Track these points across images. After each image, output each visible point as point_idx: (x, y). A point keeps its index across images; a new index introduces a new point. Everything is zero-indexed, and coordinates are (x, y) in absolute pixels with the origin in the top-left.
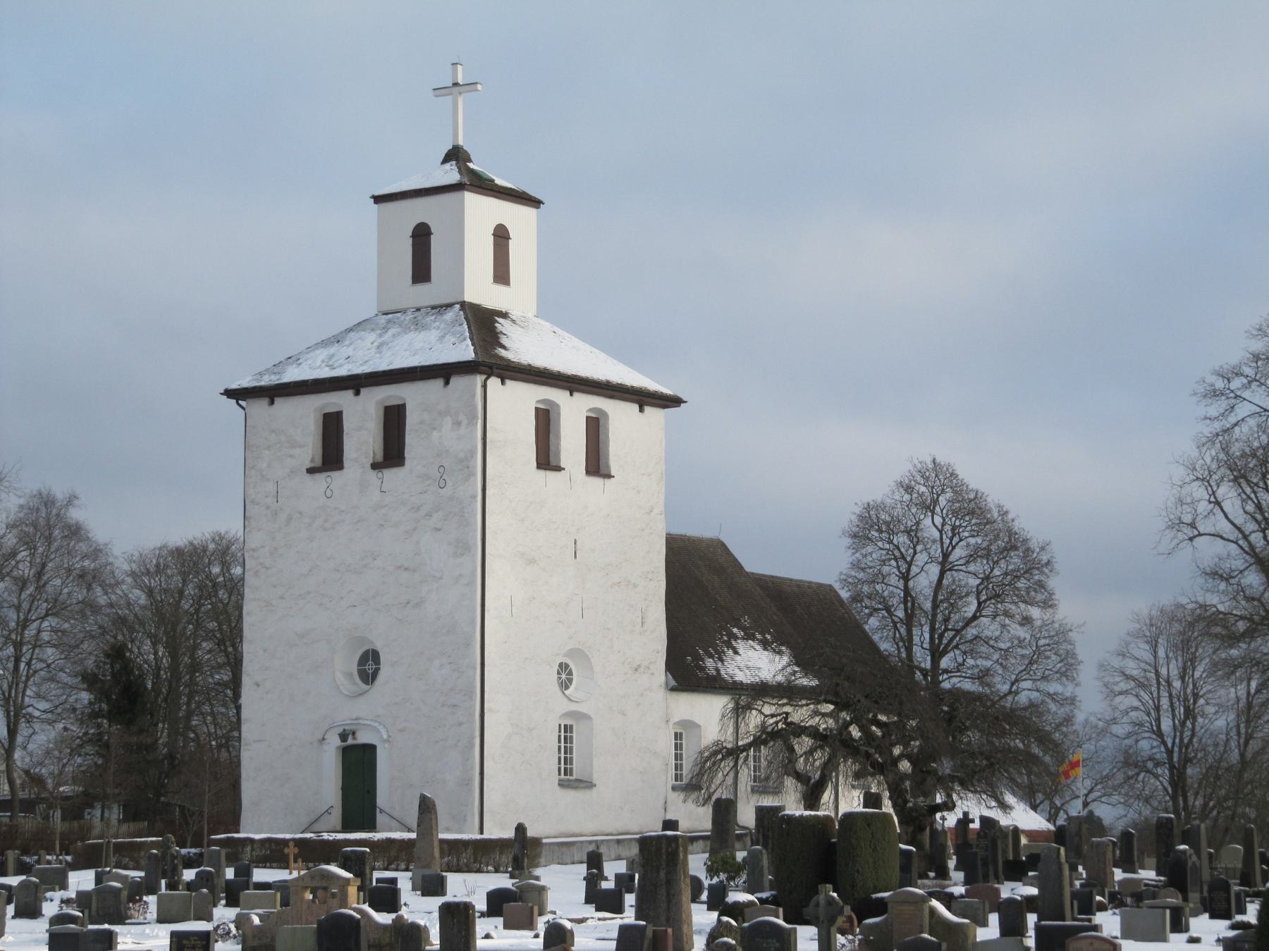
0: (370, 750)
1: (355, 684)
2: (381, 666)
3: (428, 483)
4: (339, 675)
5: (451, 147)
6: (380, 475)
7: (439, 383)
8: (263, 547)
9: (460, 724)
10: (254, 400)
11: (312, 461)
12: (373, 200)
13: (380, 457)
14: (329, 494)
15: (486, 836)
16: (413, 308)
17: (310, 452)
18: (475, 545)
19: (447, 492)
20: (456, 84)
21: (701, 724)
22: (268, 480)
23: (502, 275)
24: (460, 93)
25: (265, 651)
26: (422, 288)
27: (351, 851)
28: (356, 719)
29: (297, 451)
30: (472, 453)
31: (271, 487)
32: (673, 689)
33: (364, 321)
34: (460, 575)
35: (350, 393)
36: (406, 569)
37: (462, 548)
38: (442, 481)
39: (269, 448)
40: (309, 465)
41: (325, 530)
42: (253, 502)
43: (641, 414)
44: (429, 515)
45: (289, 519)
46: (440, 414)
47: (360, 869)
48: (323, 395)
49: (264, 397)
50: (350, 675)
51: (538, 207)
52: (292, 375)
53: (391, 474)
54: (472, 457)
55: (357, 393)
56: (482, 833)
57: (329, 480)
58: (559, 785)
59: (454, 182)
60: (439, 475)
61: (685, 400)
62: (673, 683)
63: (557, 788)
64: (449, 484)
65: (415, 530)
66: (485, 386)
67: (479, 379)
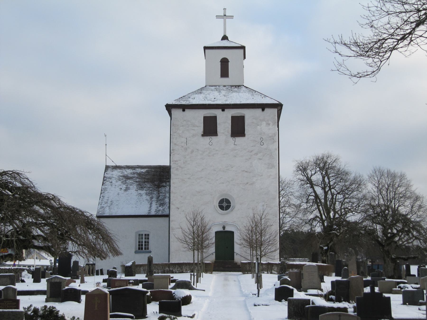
3: (256, 143)
6: (234, 139)
7: (260, 110)
8: (180, 160)
14: (211, 144)
19: (265, 146)
20: (225, 15)
22: (182, 137)
25: (181, 197)
29: (196, 128)
31: (184, 140)
36: (246, 172)
39: (183, 126)
42: (175, 144)
43: (223, 112)
44: (256, 154)
45: (192, 152)
48: (208, 110)
53: (239, 140)
54: (275, 136)
57: (211, 139)
64: (265, 144)
65: (250, 159)
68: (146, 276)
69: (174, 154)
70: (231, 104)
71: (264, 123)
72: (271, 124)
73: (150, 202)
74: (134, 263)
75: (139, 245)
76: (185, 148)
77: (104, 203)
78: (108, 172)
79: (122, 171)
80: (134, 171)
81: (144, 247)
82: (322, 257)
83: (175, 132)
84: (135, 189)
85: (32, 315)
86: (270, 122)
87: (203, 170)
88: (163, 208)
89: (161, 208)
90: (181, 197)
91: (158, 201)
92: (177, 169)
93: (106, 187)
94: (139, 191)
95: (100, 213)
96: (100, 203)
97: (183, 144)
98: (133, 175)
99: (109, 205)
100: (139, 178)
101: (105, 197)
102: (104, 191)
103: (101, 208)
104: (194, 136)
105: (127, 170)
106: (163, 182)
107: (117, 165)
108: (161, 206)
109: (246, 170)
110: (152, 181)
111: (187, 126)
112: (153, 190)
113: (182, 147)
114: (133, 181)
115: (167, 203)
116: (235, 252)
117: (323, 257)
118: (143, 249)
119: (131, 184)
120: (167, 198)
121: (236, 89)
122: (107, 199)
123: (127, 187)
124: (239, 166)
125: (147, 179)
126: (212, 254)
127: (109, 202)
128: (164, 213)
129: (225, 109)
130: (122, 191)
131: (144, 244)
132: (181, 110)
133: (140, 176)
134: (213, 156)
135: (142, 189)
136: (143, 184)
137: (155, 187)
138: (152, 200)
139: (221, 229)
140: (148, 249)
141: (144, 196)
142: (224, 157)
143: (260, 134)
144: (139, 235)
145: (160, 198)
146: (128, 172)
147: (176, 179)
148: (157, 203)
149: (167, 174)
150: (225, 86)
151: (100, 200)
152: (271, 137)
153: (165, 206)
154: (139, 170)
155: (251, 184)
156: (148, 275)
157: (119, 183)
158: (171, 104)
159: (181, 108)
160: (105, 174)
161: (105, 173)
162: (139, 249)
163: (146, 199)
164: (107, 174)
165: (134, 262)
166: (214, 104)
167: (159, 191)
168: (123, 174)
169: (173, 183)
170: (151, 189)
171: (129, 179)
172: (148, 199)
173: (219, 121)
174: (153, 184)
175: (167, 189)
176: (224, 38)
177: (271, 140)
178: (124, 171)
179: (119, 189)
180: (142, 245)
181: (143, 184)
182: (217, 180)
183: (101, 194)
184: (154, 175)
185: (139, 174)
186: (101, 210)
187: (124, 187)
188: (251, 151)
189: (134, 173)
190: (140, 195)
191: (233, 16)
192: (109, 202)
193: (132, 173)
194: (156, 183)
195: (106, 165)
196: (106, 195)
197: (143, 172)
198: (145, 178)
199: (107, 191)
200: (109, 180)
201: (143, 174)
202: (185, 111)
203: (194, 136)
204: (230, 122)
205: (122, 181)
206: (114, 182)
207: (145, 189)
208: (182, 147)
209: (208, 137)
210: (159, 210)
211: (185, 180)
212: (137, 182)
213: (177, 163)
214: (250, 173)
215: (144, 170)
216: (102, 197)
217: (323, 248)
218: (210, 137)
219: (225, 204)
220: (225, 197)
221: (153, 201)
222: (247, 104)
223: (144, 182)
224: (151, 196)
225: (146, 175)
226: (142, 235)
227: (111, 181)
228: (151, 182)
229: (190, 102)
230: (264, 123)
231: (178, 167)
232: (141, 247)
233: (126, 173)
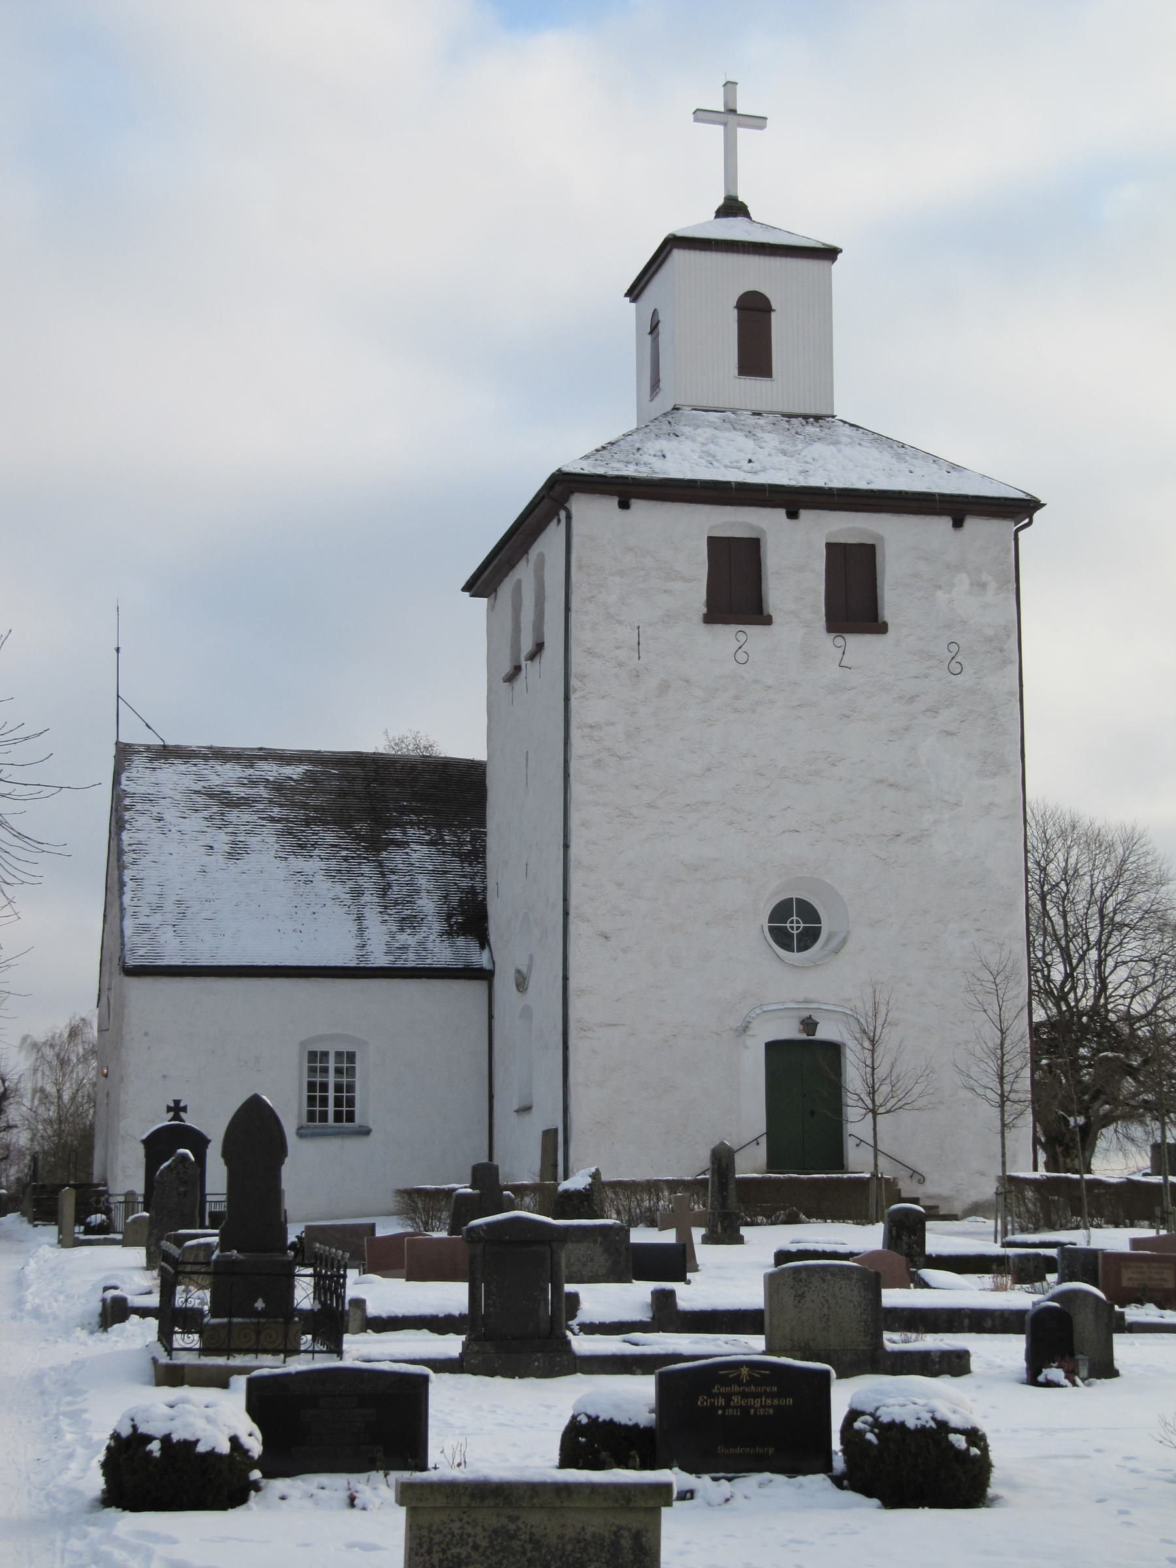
6: (839, 641)
8: (612, 724)
22: (620, 622)
25: (619, 885)
28: (806, 1001)
29: (678, 586)
34: (991, 804)
35: (779, 515)
36: (891, 785)
39: (621, 573)
41: (736, 711)
42: (590, 652)
43: (793, 522)
44: (933, 711)
45: (664, 688)
48: (729, 509)
53: (859, 645)
57: (742, 637)
65: (907, 729)
68: (703, 1237)
69: (583, 697)
70: (831, 489)
71: (963, 581)
72: (993, 585)
73: (354, 909)
74: (596, 1176)
75: (311, 1100)
77: (147, 911)
79: (195, 769)
80: (251, 771)
81: (331, 1109)
82: (1065, 1158)
83: (590, 599)
84: (273, 853)
85: (951, 1446)
86: (985, 577)
87: (709, 770)
88: (418, 937)
89: (404, 938)
91: (386, 907)
92: (599, 761)
93: (141, 836)
94: (292, 858)
95: (141, 952)
98: (251, 791)
100: (281, 806)
101: (145, 882)
102: (135, 856)
105: (218, 767)
106: (390, 824)
107: (170, 742)
108: (409, 931)
110: (340, 818)
111: (642, 573)
112: (353, 858)
113: (621, 665)
114: (255, 817)
115: (430, 918)
118: (327, 1121)
119: (248, 828)
120: (424, 894)
121: (810, 429)
122: (158, 890)
123: (233, 842)
124: (862, 761)
125: (316, 809)
126: (756, 1141)
128: (428, 961)
130: (218, 860)
131: (331, 1094)
133: (282, 795)
134: (754, 711)
135: (305, 852)
136: (304, 831)
137: (358, 844)
138: (362, 902)
139: (790, 1031)
140: (351, 1117)
141: (322, 885)
142: (800, 717)
143: (945, 627)
144: (312, 1055)
145: (395, 893)
146: (227, 775)
148: (386, 917)
149: (397, 790)
150: (760, 414)
152: (989, 640)
153: (425, 929)
154: (271, 770)
156: (716, 1232)
157: (196, 822)
159: (610, 493)
162: (311, 1117)
163: (331, 895)
165: (597, 1170)
166: (763, 485)
167: (381, 865)
168: (202, 783)
169: (583, 825)
170: (344, 853)
171: (237, 806)
172: (343, 896)
173: (773, 560)
174: (347, 833)
175: (415, 855)
176: (731, 207)
178: (204, 768)
179: (203, 850)
180: (324, 1101)
181: (304, 831)
184: (342, 794)
185: (278, 787)
187: (222, 840)
188: (912, 699)
189: (253, 783)
190: (302, 878)
191: (765, 118)
192: (169, 905)
193: (245, 781)
194: (362, 827)
195: (117, 743)
197: (291, 779)
198: (305, 806)
199: (149, 858)
200: (147, 806)
201: (293, 789)
204: (821, 566)
205: (206, 814)
206: (171, 815)
207: (317, 852)
208: (621, 665)
209: (733, 628)
210: (404, 948)
212: (272, 820)
214: (907, 789)
215: (295, 771)
218: (741, 627)
219: (795, 925)
221: (364, 906)
222: (900, 492)
223: (308, 822)
224: (350, 884)
225: (308, 792)
226: (325, 1055)
227: (155, 810)
228: (335, 823)
230: (963, 581)
232: (345, 1109)
233: (215, 781)
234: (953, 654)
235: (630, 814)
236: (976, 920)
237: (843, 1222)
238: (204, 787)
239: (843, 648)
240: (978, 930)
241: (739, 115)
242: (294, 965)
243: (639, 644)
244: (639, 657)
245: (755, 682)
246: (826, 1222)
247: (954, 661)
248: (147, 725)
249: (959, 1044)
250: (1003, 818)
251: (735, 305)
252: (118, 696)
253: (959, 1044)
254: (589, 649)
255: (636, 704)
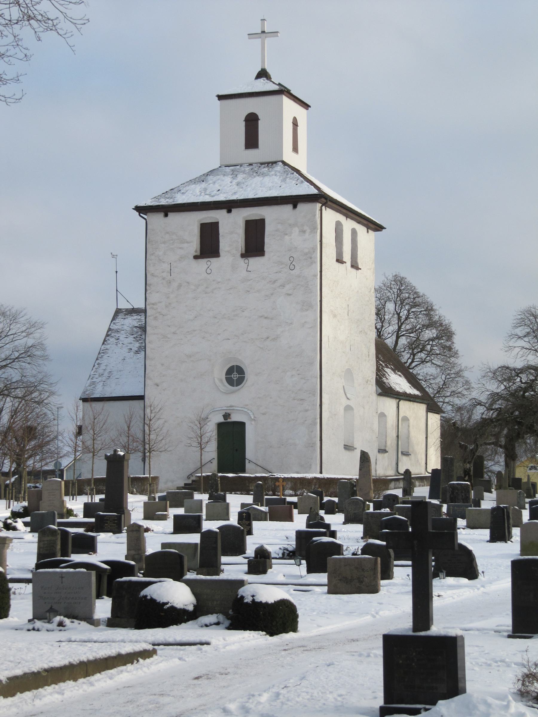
0: (241, 425)
1: (225, 386)
2: (246, 375)
3: (281, 267)
4: (217, 381)
5: (260, 70)
6: (246, 261)
7: (290, 207)
8: (161, 302)
9: (307, 411)
10: (153, 214)
11: (196, 251)
12: (217, 98)
13: (198, 253)
14: (209, 271)
15: (326, 475)
16: (247, 164)
17: (195, 246)
18: (317, 304)
19: (296, 272)
20: (263, 32)
21: (387, 415)
22: (164, 262)
23: (295, 149)
24: (266, 37)
25: (162, 365)
26: (252, 152)
27: (458, 484)
28: (230, 407)
29: (185, 245)
30: (314, 249)
31: (166, 266)
32: (380, 395)
33: (213, 170)
34: (305, 322)
35: (224, 212)
36: (266, 318)
37: (306, 306)
38: (292, 266)
39: (164, 243)
40: (195, 254)
41: (206, 293)
42: (153, 275)
44: (283, 286)
45: (180, 286)
46: (290, 225)
47: (466, 495)
49: (161, 212)
50: (221, 380)
51: (307, 109)
52: (181, 199)
53: (255, 262)
54: (314, 252)
55: (229, 211)
56: (321, 473)
57: (209, 263)
58: (344, 448)
59: (277, 89)
60: (290, 262)
61: (385, 227)
62: (380, 391)
63: (343, 449)
64: (297, 267)
65: (272, 294)
66: (321, 210)
67: (319, 205)
71: (296, 230)
76: (169, 282)
78: (117, 321)
79: (140, 317)
83: (152, 254)
86: (306, 228)
87: (196, 317)
90: (162, 365)
92: (156, 317)
95: (87, 393)
96: (91, 377)
97: (164, 275)
99: (104, 379)
101: (102, 365)
103: (90, 386)
104: (182, 258)
109: (266, 315)
111: (172, 242)
116: (246, 458)
117: (465, 465)
124: (254, 309)
126: (210, 461)
127: (106, 374)
129: (232, 209)
130: (132, 353)
132: (162, 215)
143: (288, 250)
147: (155, 334)
151: (93, 371)
152: (306, 254)
155: (274, 339)
157: (131, 339)
158: (143, 205)
159: (160, 211)
160: (112, 325)
161: (112, 323)
164: (114, 324)
173: (222, 230)
177: (307, 259)
182: (219, 334)
183: (97, 359)
186: (90, 387)
196: (104, 361)
199: (107, 355)
202: (169, 215)
203: (182, 258)
205: (135, 336)
206: (122, 336)
208: (164, 279)
211: (169, 336)
213: (155, 307)
216: (96, 366)
217: (466, 447)
220: (235, 364)
222: (265, 198)
229: (175, 200)
230: (296, 230)
231: (158, 315)
234: (292, 262)
235: (167, 337)
236: (298, 370)
237: (235, 494)
238: (140, 325)
239: (247, 264)
240: (299, 374)
241: (267, 33)
242: (138, 395)
243: (171, 270)
244: (171, 275)
245: (214, 281)
246: (231, 494)
247: (291, 265)
248: (127, 301)
249: (290, 421)
250: (309, 328)
251: (244, 120)
252: (117, 290)
253: (290, 421)
254: (153, 274)
255: (169, 294)
